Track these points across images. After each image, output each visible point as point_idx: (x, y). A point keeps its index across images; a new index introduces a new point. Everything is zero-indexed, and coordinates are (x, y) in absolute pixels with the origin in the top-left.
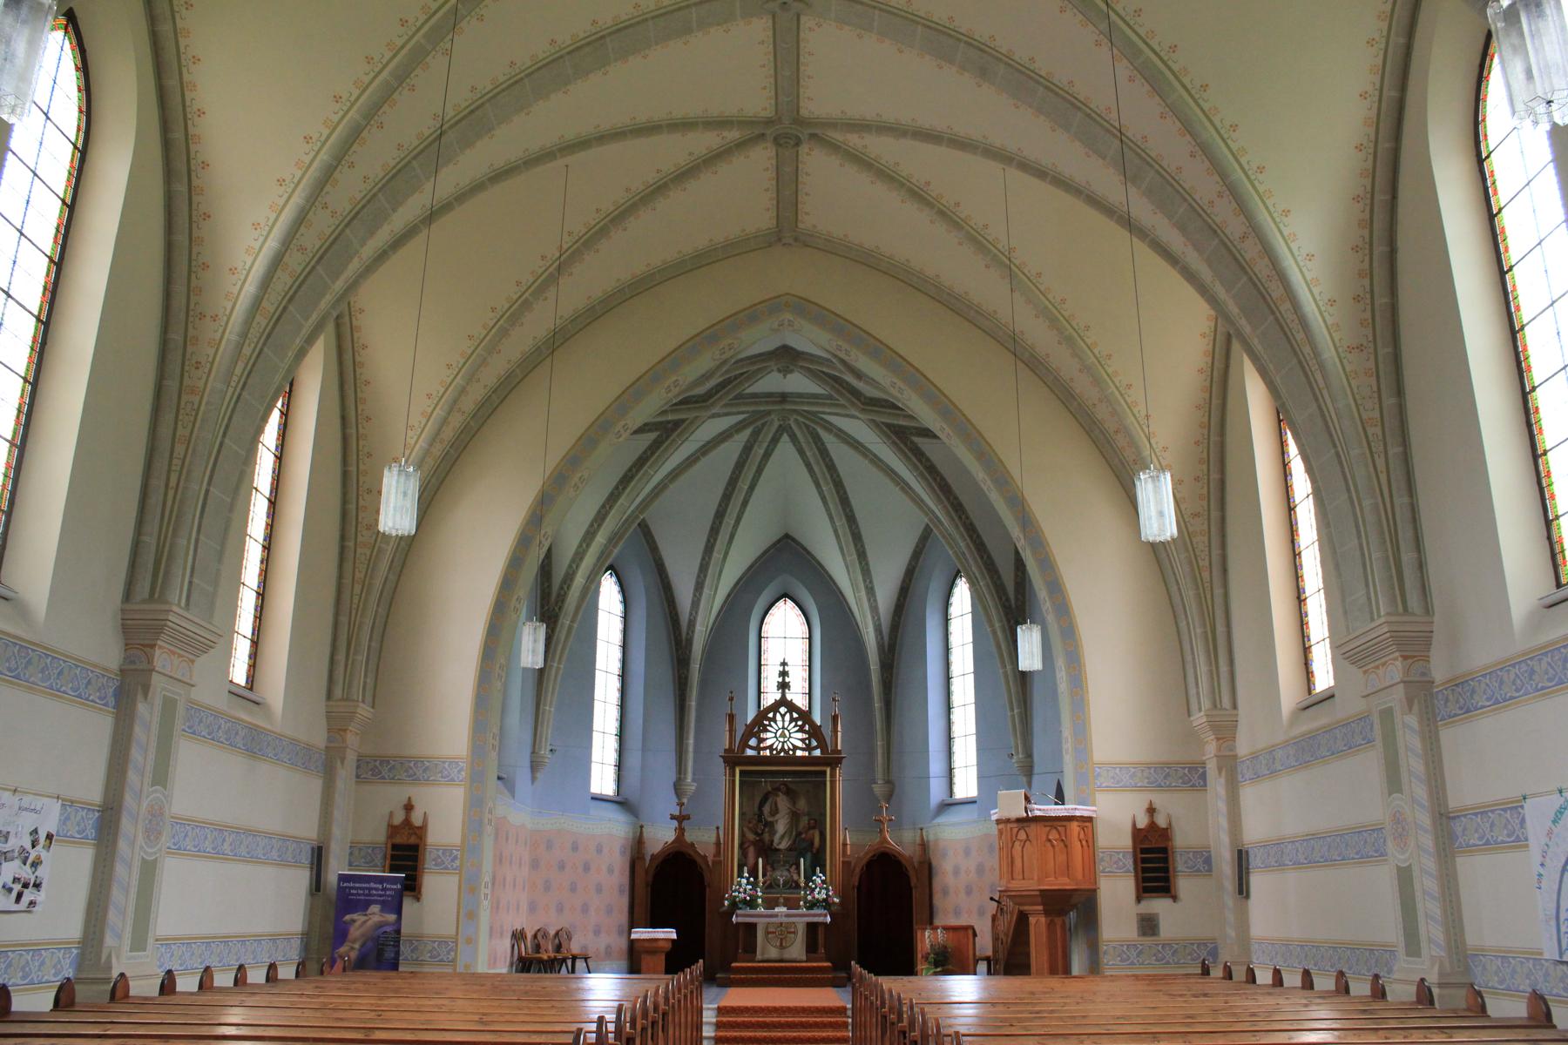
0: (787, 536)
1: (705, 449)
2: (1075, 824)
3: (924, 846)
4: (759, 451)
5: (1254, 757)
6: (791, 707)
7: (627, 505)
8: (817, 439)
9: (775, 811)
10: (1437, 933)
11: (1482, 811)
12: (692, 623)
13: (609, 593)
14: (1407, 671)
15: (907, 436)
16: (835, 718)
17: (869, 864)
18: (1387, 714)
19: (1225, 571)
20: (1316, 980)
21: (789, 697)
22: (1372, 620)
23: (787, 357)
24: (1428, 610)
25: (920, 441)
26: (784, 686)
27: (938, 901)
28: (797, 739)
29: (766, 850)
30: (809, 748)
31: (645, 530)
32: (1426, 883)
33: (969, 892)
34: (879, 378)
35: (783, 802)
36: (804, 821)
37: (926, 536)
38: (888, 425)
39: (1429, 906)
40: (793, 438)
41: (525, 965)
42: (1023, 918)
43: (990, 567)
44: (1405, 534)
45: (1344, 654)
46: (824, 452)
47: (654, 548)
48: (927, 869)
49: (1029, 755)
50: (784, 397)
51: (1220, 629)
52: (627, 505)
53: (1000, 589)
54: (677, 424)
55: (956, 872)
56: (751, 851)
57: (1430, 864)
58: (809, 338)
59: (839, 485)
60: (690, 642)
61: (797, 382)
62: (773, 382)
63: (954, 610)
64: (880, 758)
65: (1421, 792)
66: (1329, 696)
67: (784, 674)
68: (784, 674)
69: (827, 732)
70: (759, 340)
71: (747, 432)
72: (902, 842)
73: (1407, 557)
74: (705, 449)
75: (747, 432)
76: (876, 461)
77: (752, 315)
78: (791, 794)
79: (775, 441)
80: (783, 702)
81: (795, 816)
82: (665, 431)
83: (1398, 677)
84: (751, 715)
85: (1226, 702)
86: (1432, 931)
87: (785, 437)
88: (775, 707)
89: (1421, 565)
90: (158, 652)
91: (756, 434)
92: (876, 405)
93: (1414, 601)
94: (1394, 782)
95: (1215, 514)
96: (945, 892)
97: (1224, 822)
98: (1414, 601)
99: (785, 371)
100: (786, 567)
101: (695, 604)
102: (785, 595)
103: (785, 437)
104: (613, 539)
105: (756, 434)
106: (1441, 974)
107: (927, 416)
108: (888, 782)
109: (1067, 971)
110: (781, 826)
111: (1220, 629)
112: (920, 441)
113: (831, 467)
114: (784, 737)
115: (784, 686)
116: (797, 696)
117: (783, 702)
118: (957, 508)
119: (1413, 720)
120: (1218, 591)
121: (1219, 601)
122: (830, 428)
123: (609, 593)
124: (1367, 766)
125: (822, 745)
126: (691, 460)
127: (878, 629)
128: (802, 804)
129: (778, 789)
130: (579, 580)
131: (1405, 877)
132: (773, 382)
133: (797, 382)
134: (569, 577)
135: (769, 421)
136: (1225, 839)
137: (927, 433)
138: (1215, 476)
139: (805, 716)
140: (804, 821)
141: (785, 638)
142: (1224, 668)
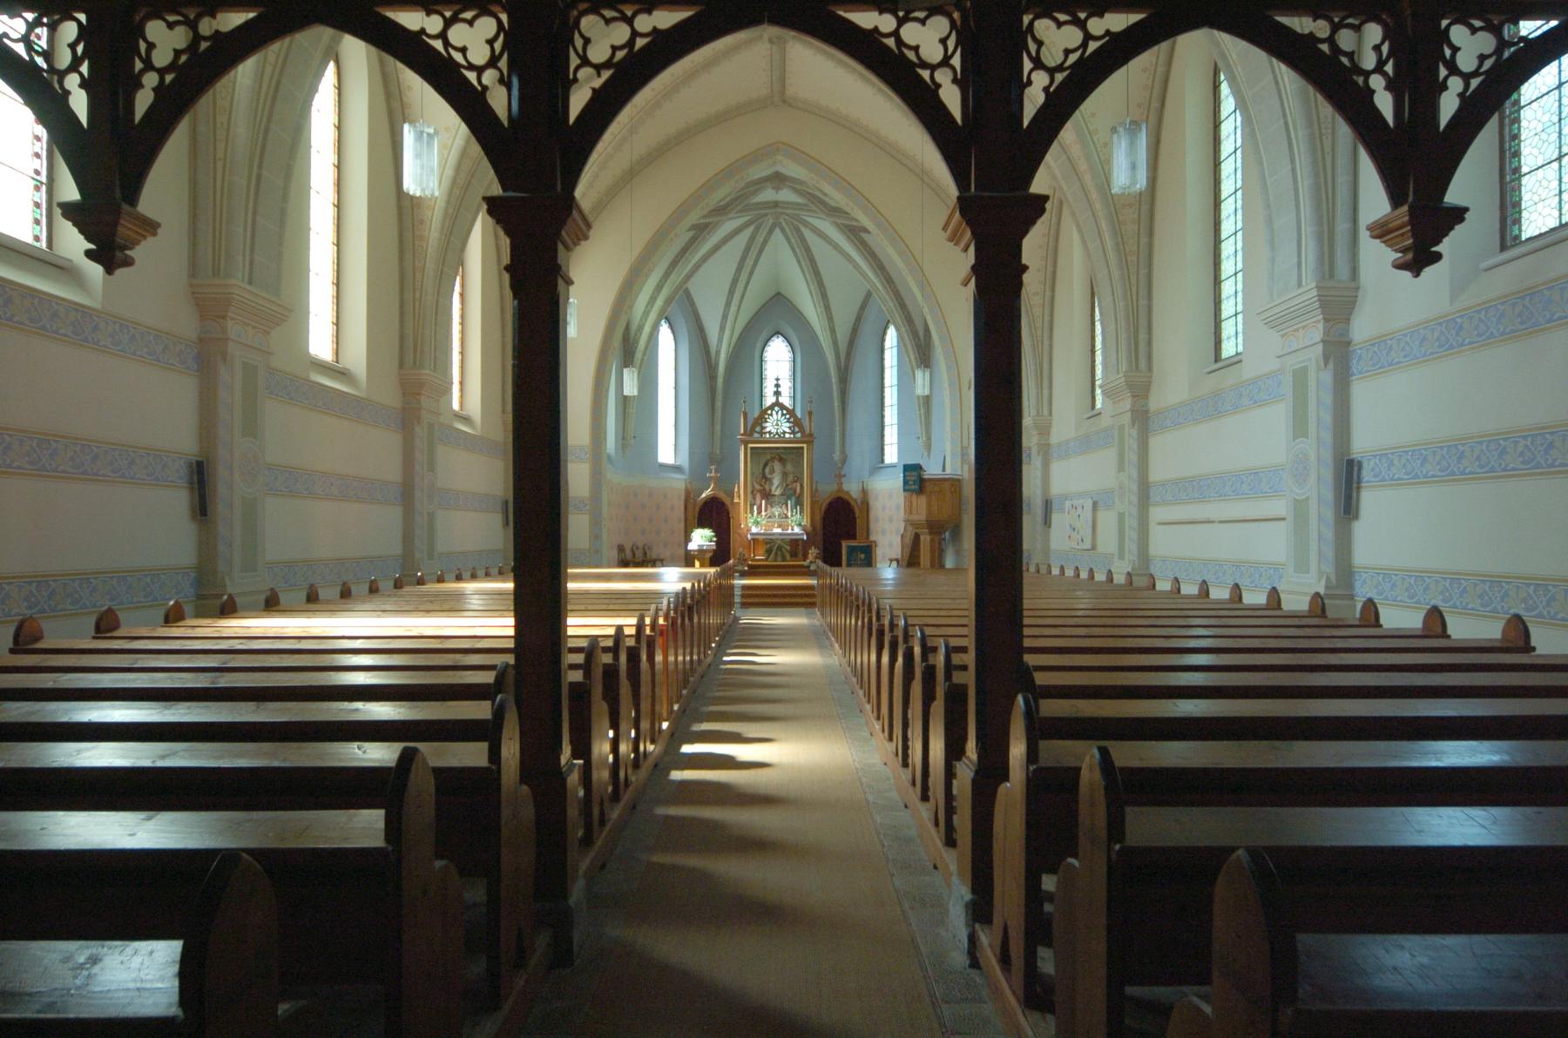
0: (779, 294)
1: (725, 241)
2: (947, 485)
3: (864, 492)
4: (760, 239)
5: (1059, 445)
6: (782, 407)
7: (675, 279)
8: (798, 230)
9: (773, 471)
10: (1134, 548)
11: (1163, 484)
12: (718, 353)
13: (665, 333)
14: (1326, 333)
15: (855, 232)
16: (810, 413)
17: (830, 504)
18: (1121, 428)
19: (1051, 329)
20: (1245, 595)
21: (781, 400)
22: (1300, 285)
23: (779, 180)
24: (1150, 368)
25: (864, 236)
26: (777, 393)
27: (872, 526)
28: (785, 427)
29: (767, 495)
30: (793, 432)
31: (688, 294)
32: (1132, 522)
33: (891, 520)
34: (836, 197)
35: (777, 466)
36: (791, 478)
37: (869, 295)
38: (846, 226)
39: (1131, 535)
40: (783, 230)
41: (1350, 463)
42: (917, 537)
43: (909, 320)
44: (1143, 322)
45: (1259, 317)
46: (803, 240)
47: (692, 304)
48: (866, 506)
49: (929, 438)
50: (776, 204)
51: (1046, 366)
52: (675, 279)
53: (914, 333)
54: (706, 226)
55: (884, 509)
56: (758, 496)
57: (1134, 511)
58: (792, 169)
59: (812, 261)
60: (717, 364)
61: (786, 195)
62: (768, 195)
63: (888, 344)
64: (838, 439)
65: (1134, 473)
66: (1237, 360)
67: (777, 386)
68: (777, 386)
69: (806, 423)
70: (760, 171)
71: (751, 229)
72: (852, 488)
73: (1143, 336)
74: (725, 241)
75: (751, 229)
76: (836, 247)
77: (754, 158)
78: (781, 460)
79: (771, 232)
80: (777, 404)
81: (785, 475)
82: (701, 230)
83: (1128, 407)
84: (756, 415)
85: (1046, 412)
86: (1132, 547)
87: (777, 230)
88: (772, 407)
89: (1149, 342)
90: (230, 323)
91: (757, 229)
92: (834, 212)
93: (1143, 364)
94: (1121, 467)
95: (1048, 293)
96: (877, 520)
97: (1039, 482)
98: (1143, 364)
99: (777, 189)
100: (775, 314)
101: (720, 340)
102: (778, 333)
103: (777, 230)
104: (668, 302)
105: (757, 229)
106: (1327, 587)
107: (865, 222)
108: (843, 452)
109: (942, 566)
110: (776, 482)
111: (1046, 366)
112: (864, 236)
113: (808, 250)
114: (777, 425)
115: (777, 393)
116: (786, 400)
117: (777, 404)
118: (889, 281)
119: (1134, 432)
120: (1046, 342)
121: (1046, 347)
122: (806, 224)
123: (665, 333)
124: (1109, 456)
125: (802, 430)
126: (716, 248)
127: (838, 356)
128: (789, 467)
129: (772, 459)
130: (647, 329)
131: (1121, 517)
132: (768, 195)
133: (786, 195)
134: (640, 328)
135: (765, 219)
136: (1039, 493)
137: (866, 231)
138: (1050, 269)
139: (791, 412)
140: (791, 478)
141: (778, 359)
142: (1046, 391)
